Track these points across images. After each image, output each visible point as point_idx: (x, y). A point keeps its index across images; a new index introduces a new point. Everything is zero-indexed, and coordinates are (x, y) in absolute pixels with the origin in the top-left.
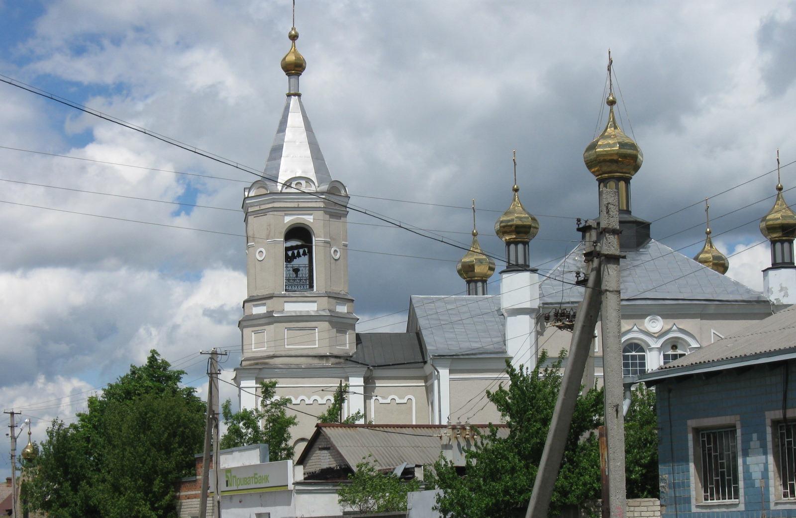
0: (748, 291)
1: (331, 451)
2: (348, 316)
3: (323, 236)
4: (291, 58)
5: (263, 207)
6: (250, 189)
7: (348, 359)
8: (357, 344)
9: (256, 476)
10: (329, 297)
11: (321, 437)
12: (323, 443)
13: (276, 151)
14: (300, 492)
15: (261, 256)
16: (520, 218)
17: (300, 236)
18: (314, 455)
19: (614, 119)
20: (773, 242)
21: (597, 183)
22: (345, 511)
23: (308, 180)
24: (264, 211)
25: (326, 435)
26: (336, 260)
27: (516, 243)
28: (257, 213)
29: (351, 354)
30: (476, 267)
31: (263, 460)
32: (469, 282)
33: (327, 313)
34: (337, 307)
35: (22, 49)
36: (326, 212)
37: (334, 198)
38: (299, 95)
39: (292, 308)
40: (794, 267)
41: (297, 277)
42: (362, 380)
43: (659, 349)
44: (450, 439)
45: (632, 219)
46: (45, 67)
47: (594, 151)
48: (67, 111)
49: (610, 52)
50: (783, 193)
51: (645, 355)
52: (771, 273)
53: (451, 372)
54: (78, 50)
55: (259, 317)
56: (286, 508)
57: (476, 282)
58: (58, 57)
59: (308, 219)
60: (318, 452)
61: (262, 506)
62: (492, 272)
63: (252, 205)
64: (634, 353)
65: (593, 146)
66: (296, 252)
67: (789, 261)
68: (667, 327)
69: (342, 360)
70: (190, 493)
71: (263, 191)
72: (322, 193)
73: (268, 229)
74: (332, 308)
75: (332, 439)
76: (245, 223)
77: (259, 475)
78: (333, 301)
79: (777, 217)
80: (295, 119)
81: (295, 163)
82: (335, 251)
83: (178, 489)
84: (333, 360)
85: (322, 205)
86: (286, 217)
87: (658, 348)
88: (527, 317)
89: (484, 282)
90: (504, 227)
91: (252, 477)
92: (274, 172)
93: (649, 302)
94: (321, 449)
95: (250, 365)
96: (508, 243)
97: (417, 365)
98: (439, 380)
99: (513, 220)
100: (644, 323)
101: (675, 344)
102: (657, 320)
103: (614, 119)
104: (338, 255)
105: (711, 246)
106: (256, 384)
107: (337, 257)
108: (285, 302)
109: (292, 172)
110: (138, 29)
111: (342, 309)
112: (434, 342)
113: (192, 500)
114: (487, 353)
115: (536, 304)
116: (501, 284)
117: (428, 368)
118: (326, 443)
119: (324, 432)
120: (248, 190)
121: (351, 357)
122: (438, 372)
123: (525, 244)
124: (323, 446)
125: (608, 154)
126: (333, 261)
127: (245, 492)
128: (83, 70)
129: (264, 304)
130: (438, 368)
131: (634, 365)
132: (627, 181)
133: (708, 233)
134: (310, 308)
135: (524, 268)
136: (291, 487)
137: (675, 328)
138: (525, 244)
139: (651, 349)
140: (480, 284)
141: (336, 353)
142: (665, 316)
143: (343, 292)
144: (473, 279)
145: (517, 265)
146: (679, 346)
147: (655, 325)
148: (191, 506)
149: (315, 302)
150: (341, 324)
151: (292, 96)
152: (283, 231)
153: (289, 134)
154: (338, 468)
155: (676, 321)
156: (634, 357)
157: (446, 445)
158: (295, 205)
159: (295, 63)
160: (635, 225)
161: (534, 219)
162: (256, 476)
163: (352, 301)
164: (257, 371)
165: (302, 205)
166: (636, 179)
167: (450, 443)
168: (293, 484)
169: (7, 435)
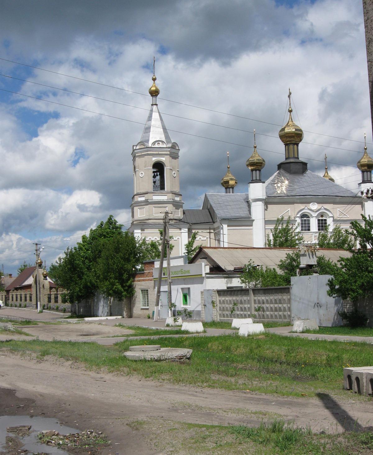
0: (352, 193)
1: (208, 259)
2: (180, 202)
3: (169, 166)
4: (153, 89)
5: (143, 153)
6: (136, 146)
7: (180, 220)
8: (183, 214)
9: (182, 270)
10: (172, 193)
11: (201, 253)
12: (203, 256)
13: (147, 129)
14: (208, 278)
15: (142, 175)
16: (258, 160)
17: (159, 167)
18: (198, 261)
19: (291, 118)
20: (363, 172)
21: (284, 146)
22: (228, 286)
23: (163, 142)
24: (144, 155)
25: (205, 252)
26: (174, 177)
27: (256, 170)
28: (139, 156)
29: (181, 219)
30: (230, 181)
31: (185, 263)
32: (226, 188)
33: (172, 200)
34: (176, 198)
35: (15, 96)
36: (171, 156)
37: (173, 151)
38: (157, 105)
39: (156, 198)
40: (372, 183)
41: (155, 185)
42: (187, 230)
43: (316, 217)
44: (305, 252)
45: (299, 161)
46: (24, 104)
47: (284, 132)
48: (32, 124)
49: (289, 89)
50: (367, 151)
51: (309, 220)
52: (362, 185)
53: (228, 226)
54: (39, 98)
55: (141, 202)
56: (200, 285)
57: (229, 188)
58: (30, 100)
59: (163, 159)
60: (200, 260)
61: (185, 284)
62: (236, 184)
63: (137, 153)
64: (305, 219)
65: (283, 129)
66: (156, 174)
67: (370, 180)
68: (319, 208)
69: (178, 221)
70: (140, 279)
71: (143, 147)
72: (169, 148)
73: (145, 163)
74: (173, 198)
75: (209, 254)
76: (132, 161)
77: (184, 270)
78: (174, 195)
79: (365, 161)
80: (155, 115)
81: (156, 135)
82: (174, 173)
83: (134, 277)
84: (174, 221)
85: (169, 153)
86: (153, 158)
87: (316, 216)
88: (261, 202)
89: (233, 188)
90: (251, 163)
91: (180, 271)
92: (147, 138)
93: (311, 196)
94: (201, 258)
95: (138, 223)
96: (252, 170)
97: (205, 223)
98: (223, 230)
99: (255, 160)
100: (309, 205)
101: (322, 215)
102: (315, 204)
103: (291, 118)
104: (175, 174)
105: (328, 174)
106: (141, 231)
107: (175, 176)
108: (153, 195)
109: (155, 138)
110: (65, 90)
111: (178, 199)
112: (220, 213)
113: (141, 282)
114: (243, 218)
115: (264, 197)
116: (249, 188)
117: (216, 225)
118: (204, 256)
119: (204, 250)
120: (136, 146)
121: (181, 220)
122: (223, 226)
123: (260, 170)
124: (202, 257)
125: (289, 133)
126: (173, 178)
127: (176, 278)
128: (41, 106)
129: (144, 196)
130: (222, 224)
131: (305, 224)
132: (297, 145)
133: (326, 169)
134: (164, 198)
135: (259, 181)
136: (204, 275)
137: (323, 208)
138: (260, 170)
139: (313, 217)
140: (231, 189)
141: (175, 218)
142: (318, 203)
143: (177, 191)
144: (228, 187)
145: (256, 180)
146: (324, 216)
147: (314, 206)
148: (141, 285)
149: (166, 195)
150: (177, 205)
151: (154, 106)
152: (152, 164)
153: (153, 122)
154: (212, 267)
155: (323, 205)
156: (305, 220)
157: (303, 254)
158: (157, 153)
159: (155, 91)
160: (302, 164)
161: (263, 160)
162: (182, 270)
163: (181, 195)
164: (142, 226)
165: (160, 153)
166: (300, 145)
167: (305, 254)
168: (205, 274)
169: (35, 254)
